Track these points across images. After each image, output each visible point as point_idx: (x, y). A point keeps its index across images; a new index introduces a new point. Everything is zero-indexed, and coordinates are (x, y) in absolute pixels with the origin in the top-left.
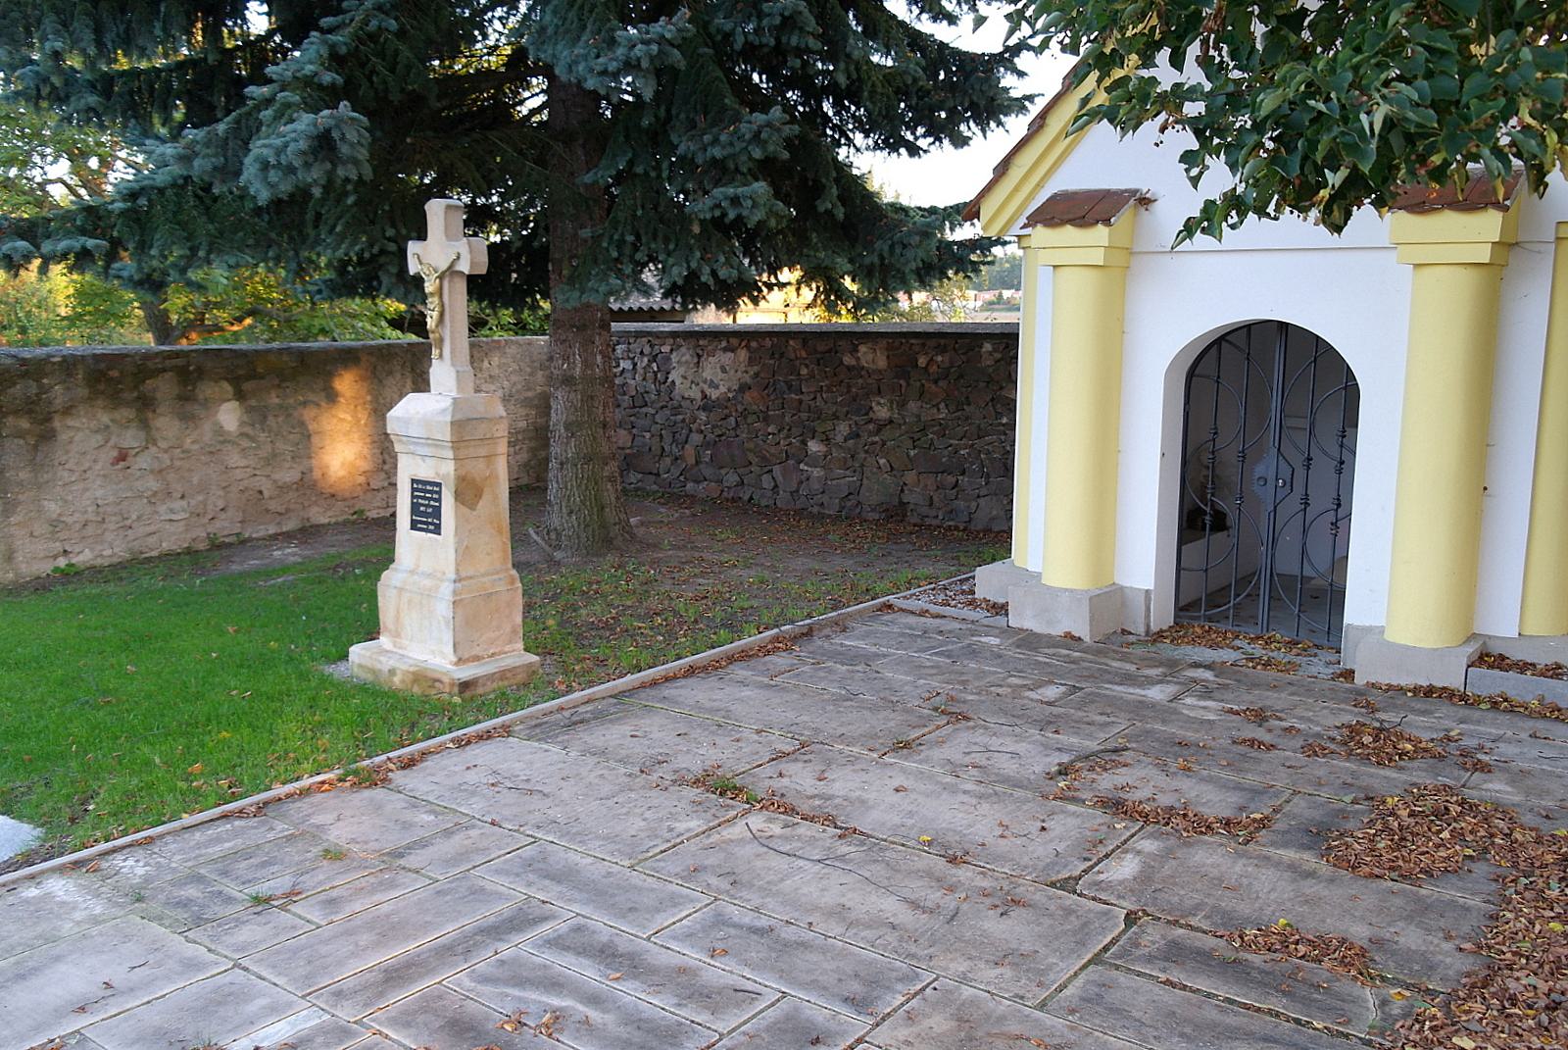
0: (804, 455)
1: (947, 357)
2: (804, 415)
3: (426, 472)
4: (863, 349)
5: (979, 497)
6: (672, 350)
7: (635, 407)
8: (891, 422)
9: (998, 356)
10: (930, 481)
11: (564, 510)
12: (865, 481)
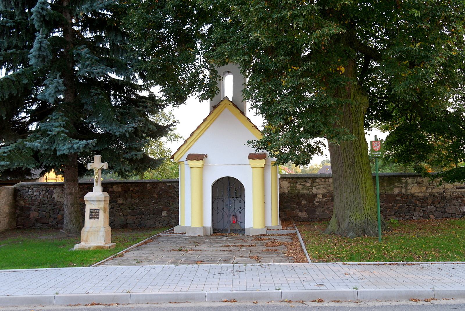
1: (138, 188)
4: (115, 187)
5: (147, 220)
6: (53, 189)
7: (40, 205)
8: (123, 204)
9: (151, 187)
11: (72, 224)
12: (116, 219)
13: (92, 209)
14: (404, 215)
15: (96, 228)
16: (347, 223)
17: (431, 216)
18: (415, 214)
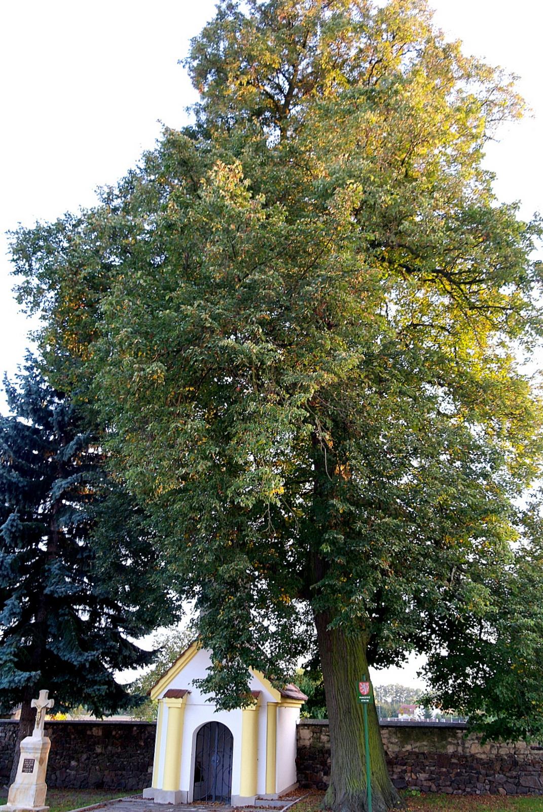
0: (68, 766)
2: (71, 752)
3: (30, 756)
4: (94, 729)
10: (113, 774)
14: (463, 787)
16: (343, 792)
17: (501, 789)
18: (479, 785)
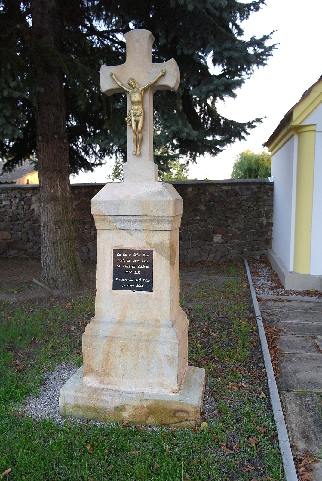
5: (188, 248)
6: (32, 196)
9: (195, 193)
13: (121, 251)
15: (142, 324)
